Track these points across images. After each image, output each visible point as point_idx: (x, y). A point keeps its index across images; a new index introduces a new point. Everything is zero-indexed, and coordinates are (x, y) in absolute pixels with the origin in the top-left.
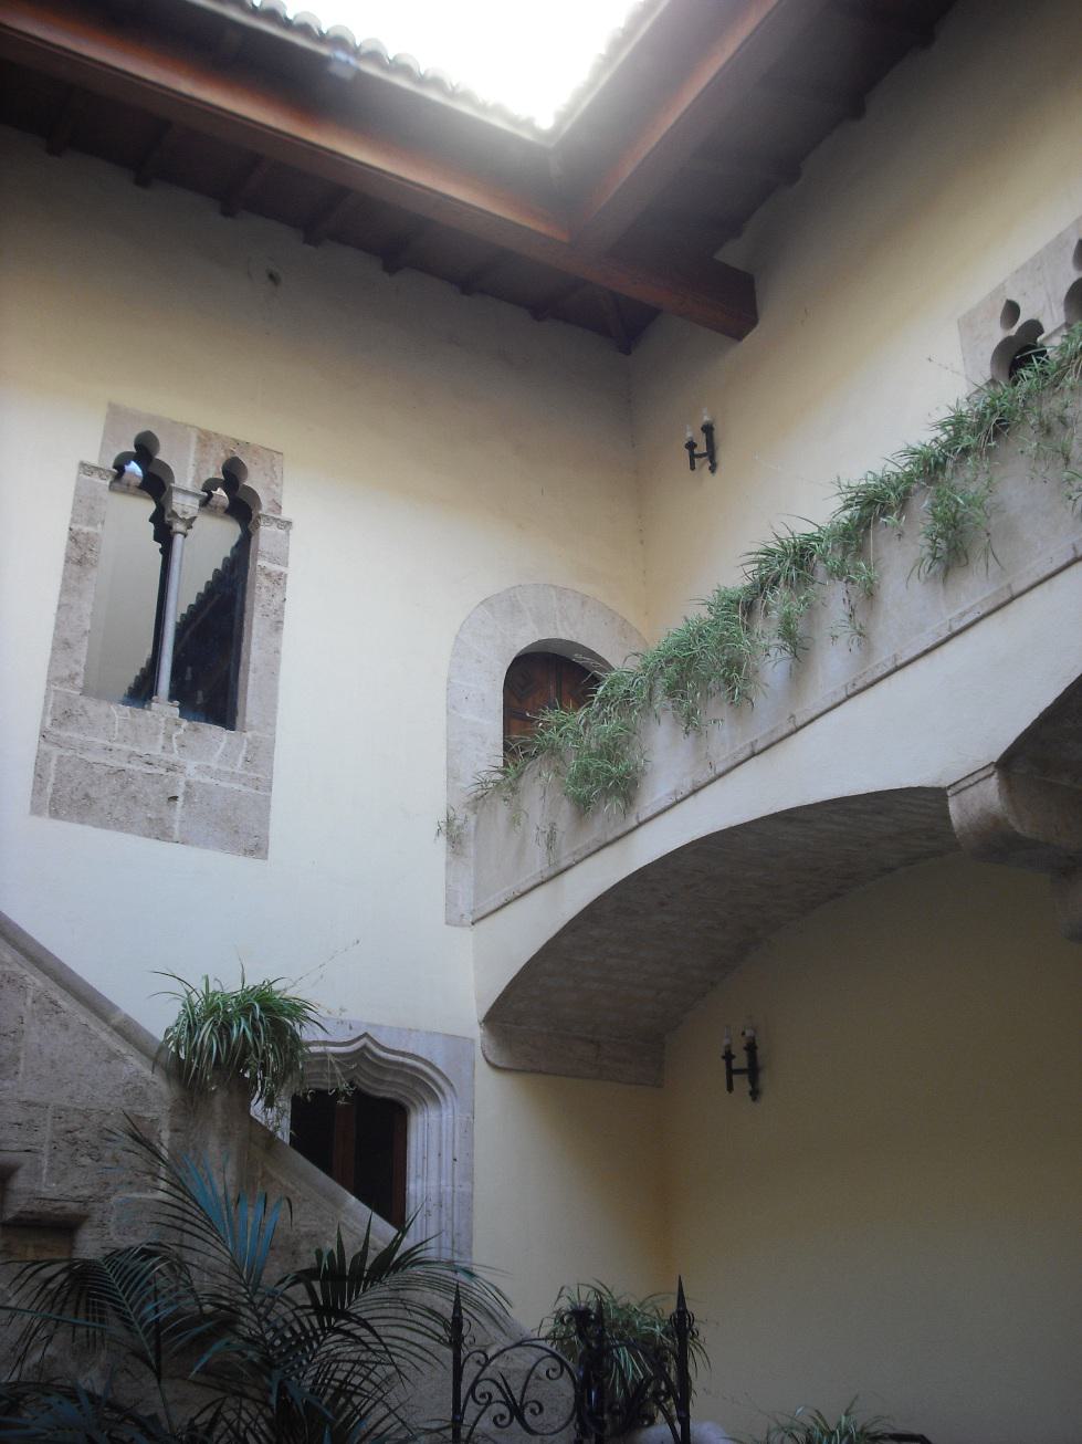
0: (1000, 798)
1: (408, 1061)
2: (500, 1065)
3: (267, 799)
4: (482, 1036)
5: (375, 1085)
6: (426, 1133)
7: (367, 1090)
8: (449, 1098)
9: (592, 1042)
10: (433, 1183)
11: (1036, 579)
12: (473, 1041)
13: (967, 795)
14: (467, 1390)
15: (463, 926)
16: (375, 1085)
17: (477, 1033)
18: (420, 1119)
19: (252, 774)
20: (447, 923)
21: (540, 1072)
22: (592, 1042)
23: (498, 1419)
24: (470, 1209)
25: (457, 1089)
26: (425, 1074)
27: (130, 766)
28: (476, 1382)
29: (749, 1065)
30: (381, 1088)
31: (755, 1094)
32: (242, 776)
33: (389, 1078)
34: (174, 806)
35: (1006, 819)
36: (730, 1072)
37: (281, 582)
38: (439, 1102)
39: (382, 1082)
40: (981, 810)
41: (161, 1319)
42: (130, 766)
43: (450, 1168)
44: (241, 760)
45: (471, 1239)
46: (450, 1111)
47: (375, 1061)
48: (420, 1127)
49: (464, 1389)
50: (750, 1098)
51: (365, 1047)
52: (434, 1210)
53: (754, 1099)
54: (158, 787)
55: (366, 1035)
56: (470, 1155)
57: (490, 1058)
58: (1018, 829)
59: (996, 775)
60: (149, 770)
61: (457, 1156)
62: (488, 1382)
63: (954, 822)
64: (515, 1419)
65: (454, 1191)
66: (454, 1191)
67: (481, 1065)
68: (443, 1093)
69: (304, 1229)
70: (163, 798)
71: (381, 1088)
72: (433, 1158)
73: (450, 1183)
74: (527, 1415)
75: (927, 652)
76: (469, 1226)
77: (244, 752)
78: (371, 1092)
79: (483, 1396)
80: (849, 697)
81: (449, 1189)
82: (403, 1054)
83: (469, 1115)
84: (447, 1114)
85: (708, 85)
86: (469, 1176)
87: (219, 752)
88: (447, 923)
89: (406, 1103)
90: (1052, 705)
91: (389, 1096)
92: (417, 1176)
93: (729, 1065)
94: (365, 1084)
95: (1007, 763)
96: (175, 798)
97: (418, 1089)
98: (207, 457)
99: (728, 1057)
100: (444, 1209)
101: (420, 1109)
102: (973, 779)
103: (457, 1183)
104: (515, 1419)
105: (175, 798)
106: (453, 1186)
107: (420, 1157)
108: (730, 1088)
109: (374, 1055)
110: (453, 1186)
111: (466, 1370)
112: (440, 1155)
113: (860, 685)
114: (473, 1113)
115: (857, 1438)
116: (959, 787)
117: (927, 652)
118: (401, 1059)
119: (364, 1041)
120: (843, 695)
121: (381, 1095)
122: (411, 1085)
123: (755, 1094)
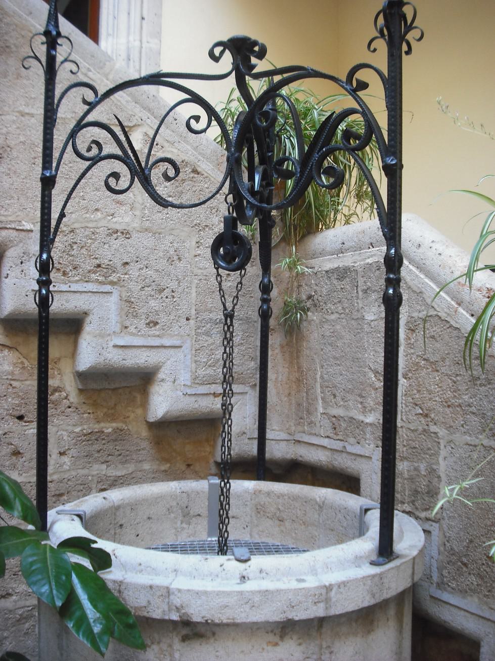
10: (123, 40)
14: (64, 138)
23: (112, 182)
28: (80, 126)
29: (277, 463)
41: (94, 546)
49: (60, 136)
61: (145, 16)
62: (74, 90)
64: (136, 179)
66: (141, 47)
74: (156, 175)
79: (89, 149)
81: (137, 43)
98: (332, 649)
100: (132, 61)
103: (144, 40)
104: (136, 179)
106: (141, 41)
110: (141, 41)
111: (61, 113)
112: (129, 14)
115: (272, 173)
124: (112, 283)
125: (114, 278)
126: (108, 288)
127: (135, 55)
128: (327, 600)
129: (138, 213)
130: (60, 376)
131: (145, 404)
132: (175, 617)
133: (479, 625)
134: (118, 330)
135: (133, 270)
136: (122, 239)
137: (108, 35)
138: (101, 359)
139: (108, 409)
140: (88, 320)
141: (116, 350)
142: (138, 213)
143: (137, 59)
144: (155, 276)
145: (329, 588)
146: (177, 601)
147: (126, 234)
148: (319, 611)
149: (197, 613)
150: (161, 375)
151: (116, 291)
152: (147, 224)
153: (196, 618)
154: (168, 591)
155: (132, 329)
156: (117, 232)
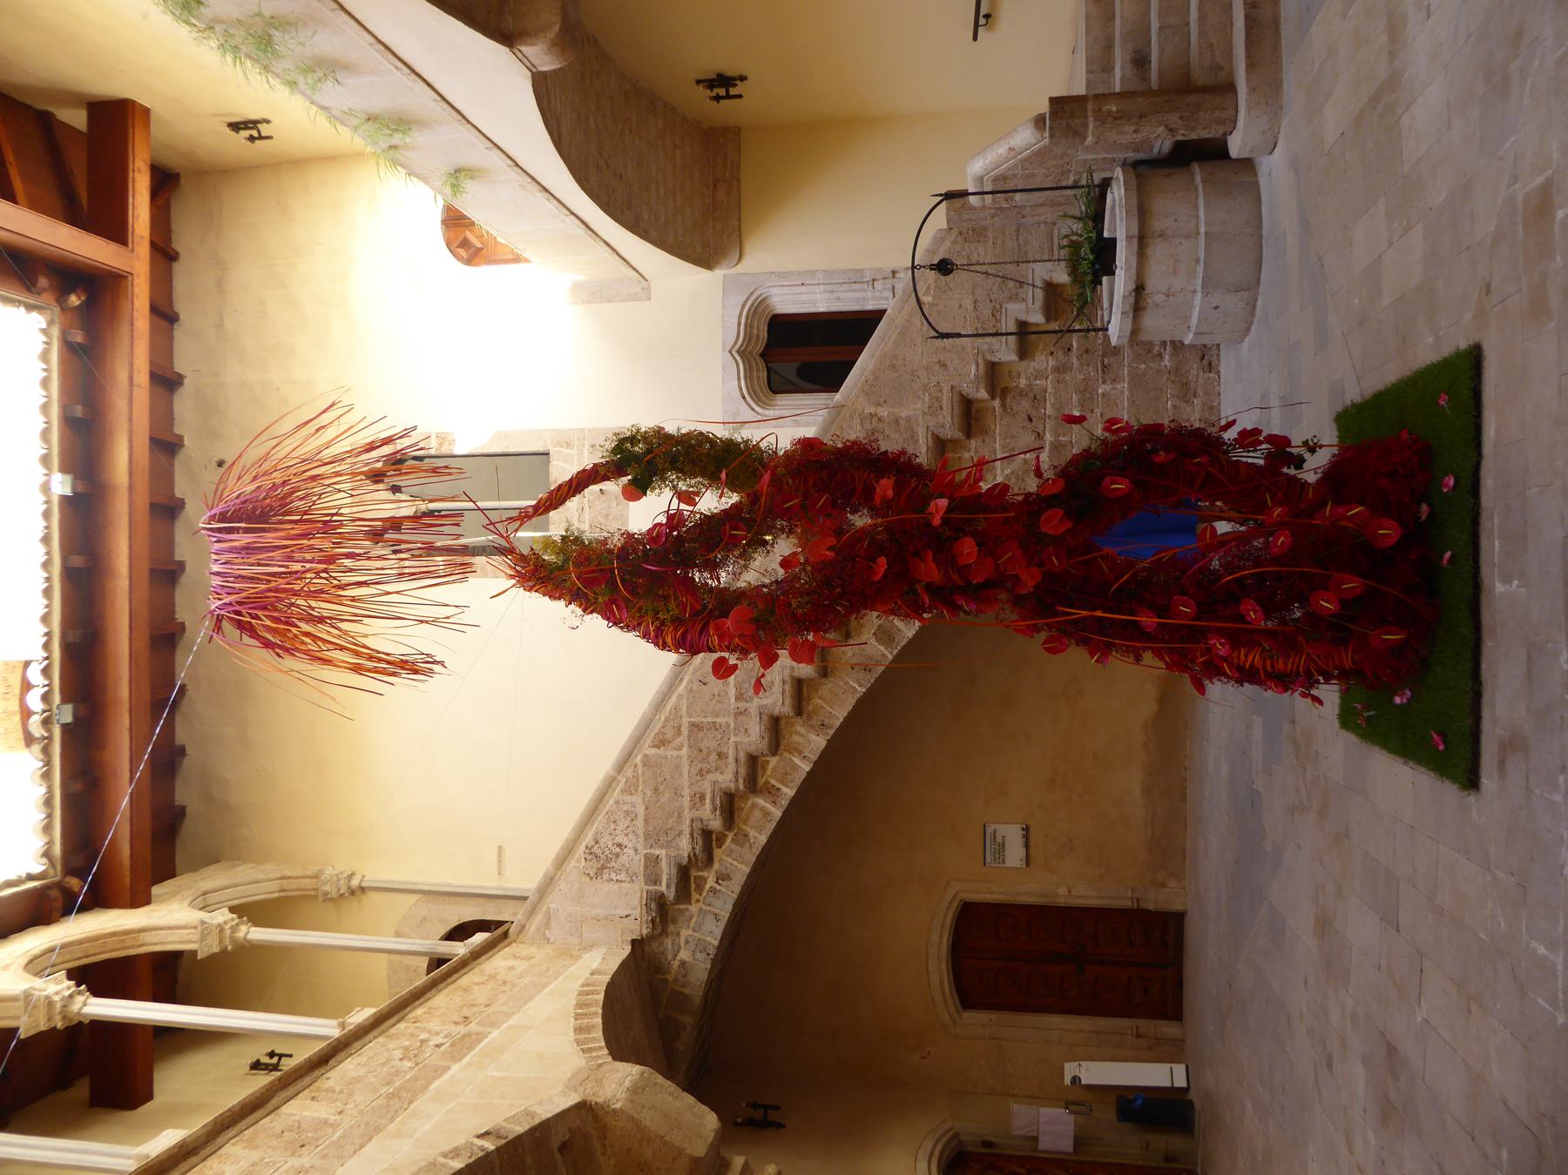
0: (535, 45)
1: (743, 321)
2: (738, 255)
3: (590, 431)
4: (720, 269)
5: (761, 340)
6: (789, 302)
7: (764, 345)
8: (763, 291)
9: (715, 186)
10: (818, 296)
11: (362, 30)
12: (725, 276)
13: (535, 61)
15: (649, 286)
16: (761, 340)
17: (719, 273)
18: (779, 307)
19: (576, 442)
20: (649, 299)
21: (739, 225)
22: (715, 186)
24: (833, 271)
25: (756, 287)
26: (749, 311)
27: (587, 521)
30: (761, 336)
31: (743, 78)
32: (578, 449)
33: (755, 331)
34: (607, 491)
35: (551, 40)
36: (728, 96)
37: (443, 436)
38: (767, 296)
39: (758, 336)
40: (546, 54)
42: (587, 521)
43: (809, 287)
44: (568, 451)
45: (853, 270)
46: (772, 289)
47: (746, 343)
48: (783, 306)
50: (745, 82)
51: (738, 352)
52: (836, 295)
53: (746, 79)
54: (596, 503)
55: (730, 352)
56: (799, 273)
57: (736, 262)
58: (557, 28)
59: (523, 48)
60: (586, 506)
63: (559, 66)
65: (823, 284)
66: (823, 284)
67: (740, 268)
68: (760, 296)
69: (858, 428)
70: (604, 497)
71: (761, 336)
72: (803, 297)
73: (817, 287)
75: (429, 85)
76: (844, 272)
77: (562, 449)
78: (765, 341)
80: (468, 122)
81: (821, 287)
82: (739, 324)
83: (773, 276)
84: (774, 291)
85: (58, 362)
86: (812, 273)
87: (564, 465)
88: (649, 299)
89: (771, 314)
90: (462, 22)
91: (766, 329)
92: (815, 306)
93: (723, 98)
94: (760, 347)
95: (507, 37)
96: (601, 490)
97: (759, 312)
99: (718, 98)
101: (772, 308)
102: (523, 60)
105: (601, 490)
107: (802, 289)
108: (740, 96)
109: (742, 345)
113: (460, 118)
114: (772, 273)
116: (530, 67)
117: (429, 85)
118: (742, 327)
119: (734, 352)
120: (469, 126)
121: (766, 334)
122: (758, 317)
123: (743, 78)
124: (1001, 307)
125: (998, 307)
126: (1003, 310)
127: (829, 288)
128: (1132, 237)
129: (964, 296)
130: (876, 433)
131: (1063, 285)
132: (1133, 294)
133: (756, 837)
134: (1024, 303)
135: (994, 297)
136: (979, 304)
137: (815, 306)
138: (1040, 311)
139: (592, 908)
140: (1020, 319)
141: (1035, 303)
142: (964, 296)
143: (833, 286)
144: (996, 285)
145: (1127, 236)
146: (1128, 294)
147: (975, 302)
148: (1135, 241)
149: (1132, 286)
150: (1048, 279)
151: (1005, 305)
152: (970, 291)
153: (1134, 287)
154: (1124, 297)
155: (1024, 296)
156: (975, 307)
